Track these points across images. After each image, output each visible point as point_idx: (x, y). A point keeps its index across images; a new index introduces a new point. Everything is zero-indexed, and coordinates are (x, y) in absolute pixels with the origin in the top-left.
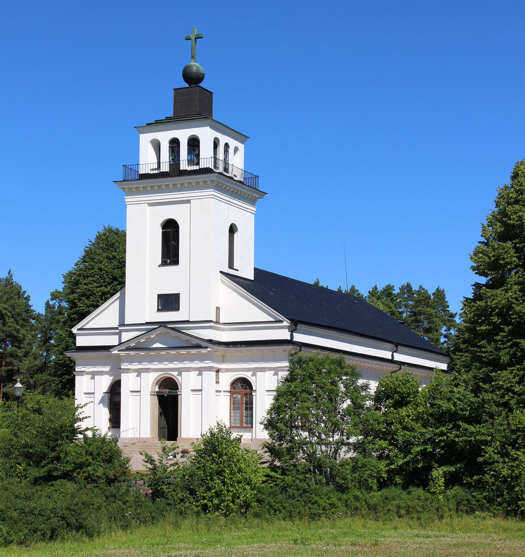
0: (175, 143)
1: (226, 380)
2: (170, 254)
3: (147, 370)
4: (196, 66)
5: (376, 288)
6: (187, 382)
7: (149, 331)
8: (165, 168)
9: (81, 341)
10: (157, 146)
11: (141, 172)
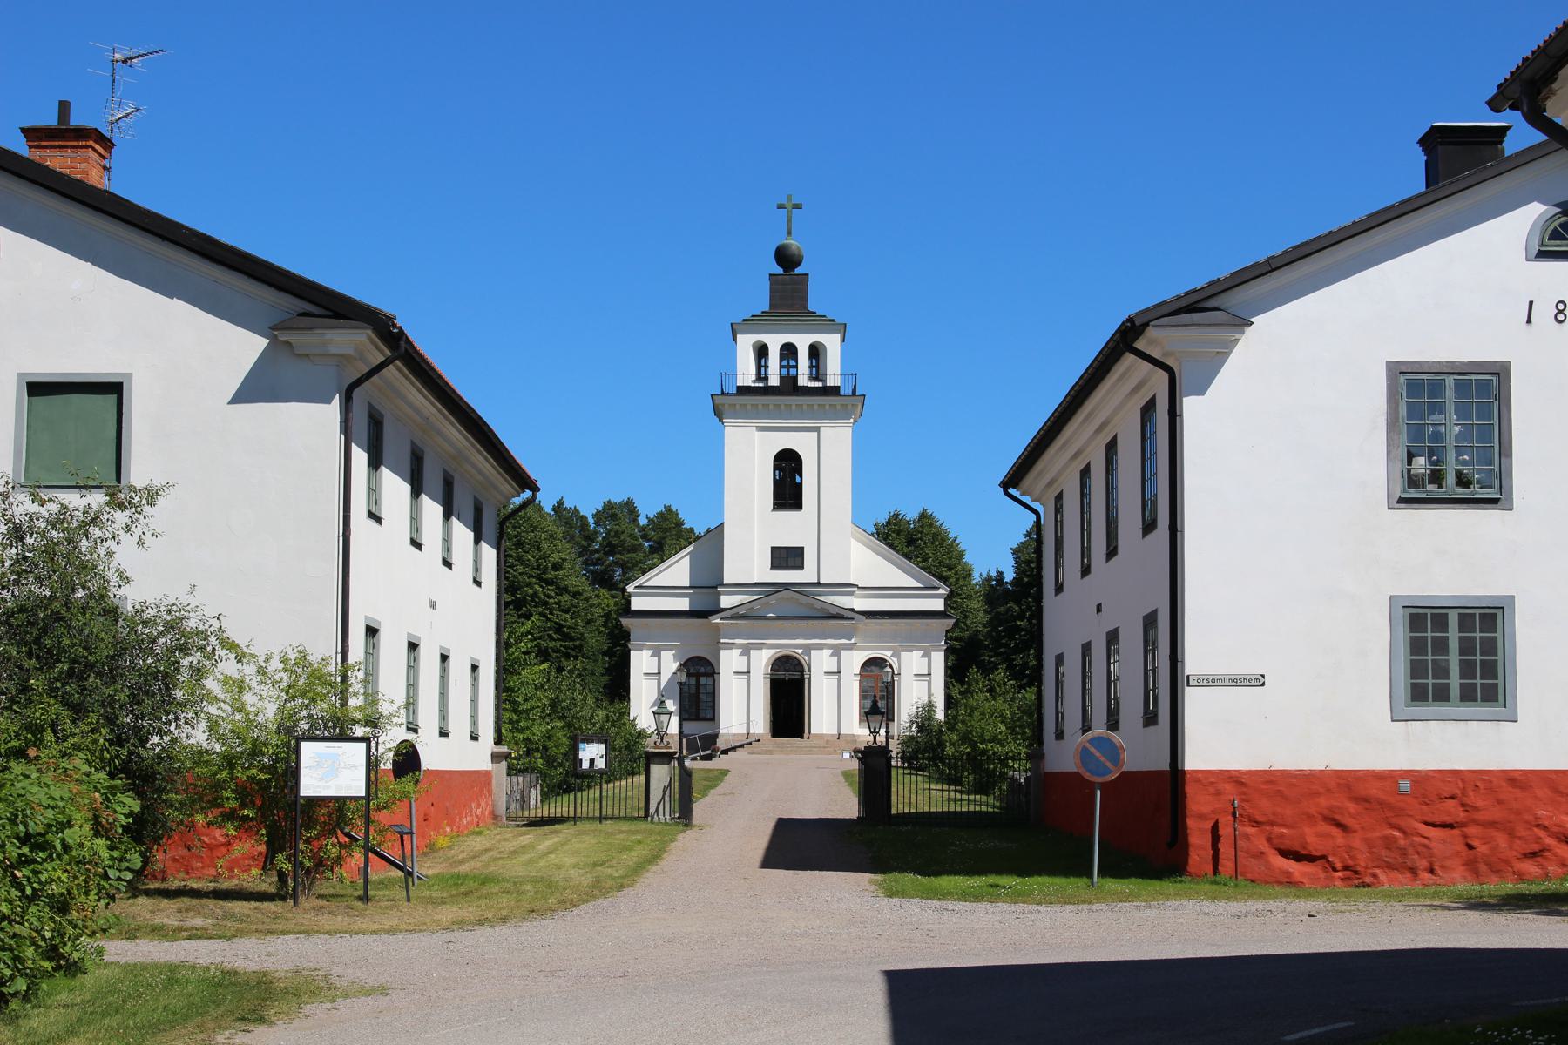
0: (789, 351)
1: (854, 660)
2: (788, 493)
3: (760, 647)
4: (793, 243)
5: (254, 389)
6: (820, 663)
7: (768, 594)
8: (774, 381)
9: (637, 604)
10: (762, 352)
11: (740, 383)
